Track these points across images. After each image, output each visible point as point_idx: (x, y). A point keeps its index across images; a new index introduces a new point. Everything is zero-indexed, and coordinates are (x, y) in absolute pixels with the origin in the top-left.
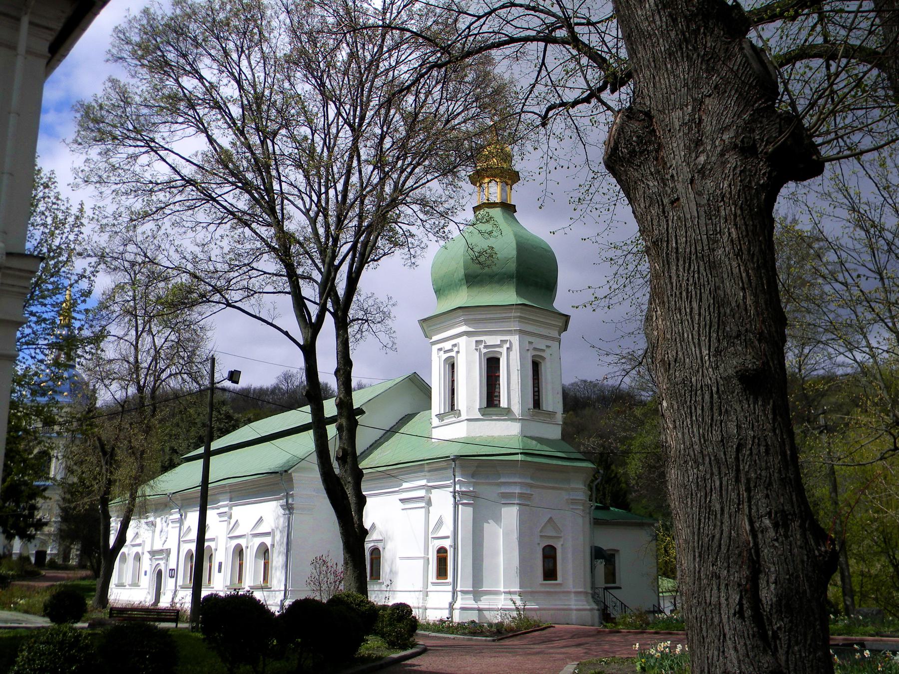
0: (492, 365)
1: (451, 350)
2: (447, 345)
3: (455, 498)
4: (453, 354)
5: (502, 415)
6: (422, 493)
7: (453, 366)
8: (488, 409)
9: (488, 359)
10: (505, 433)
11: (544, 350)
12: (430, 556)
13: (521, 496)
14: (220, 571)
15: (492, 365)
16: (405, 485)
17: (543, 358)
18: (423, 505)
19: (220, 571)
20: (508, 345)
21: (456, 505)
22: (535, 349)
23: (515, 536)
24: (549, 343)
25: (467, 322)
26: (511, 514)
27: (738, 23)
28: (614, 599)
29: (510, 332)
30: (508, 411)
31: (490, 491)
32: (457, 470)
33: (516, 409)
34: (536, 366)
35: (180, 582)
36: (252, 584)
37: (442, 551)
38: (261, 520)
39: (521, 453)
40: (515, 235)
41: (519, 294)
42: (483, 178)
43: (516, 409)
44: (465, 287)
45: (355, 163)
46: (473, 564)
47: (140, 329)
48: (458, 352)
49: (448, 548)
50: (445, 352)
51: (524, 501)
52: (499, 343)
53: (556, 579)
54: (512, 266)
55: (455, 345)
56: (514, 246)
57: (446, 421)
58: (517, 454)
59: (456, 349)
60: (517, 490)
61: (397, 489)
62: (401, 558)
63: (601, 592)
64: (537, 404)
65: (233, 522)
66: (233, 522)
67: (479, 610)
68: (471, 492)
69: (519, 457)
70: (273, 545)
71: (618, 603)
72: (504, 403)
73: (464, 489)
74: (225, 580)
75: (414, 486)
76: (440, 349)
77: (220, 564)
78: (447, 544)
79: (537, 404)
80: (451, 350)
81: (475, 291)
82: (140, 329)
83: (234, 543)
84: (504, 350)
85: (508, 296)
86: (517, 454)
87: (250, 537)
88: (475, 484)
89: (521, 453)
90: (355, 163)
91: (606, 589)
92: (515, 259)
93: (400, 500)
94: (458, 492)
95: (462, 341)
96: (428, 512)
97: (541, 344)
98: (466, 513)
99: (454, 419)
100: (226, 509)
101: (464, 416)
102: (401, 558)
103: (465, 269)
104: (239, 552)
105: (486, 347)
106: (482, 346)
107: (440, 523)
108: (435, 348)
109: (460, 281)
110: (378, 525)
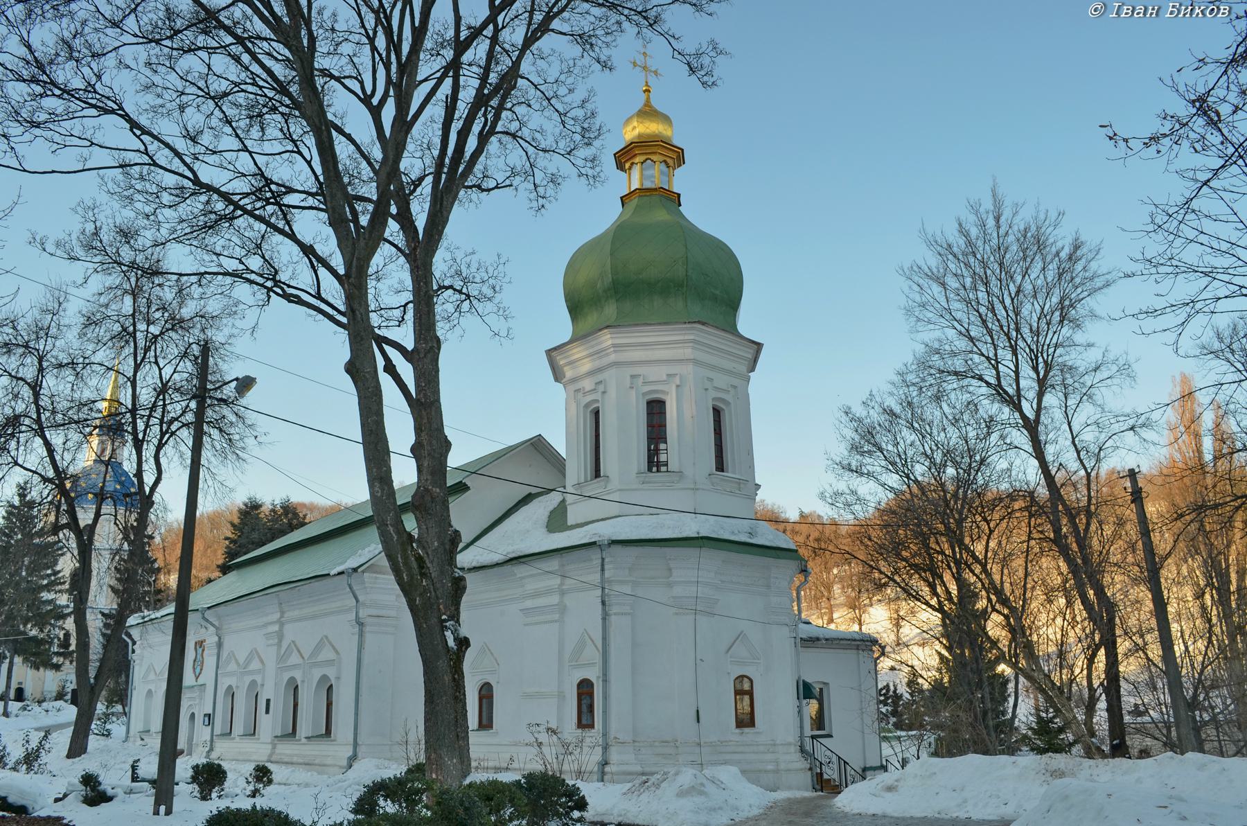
0: (656, 409)
4: (597, 396)
7: (596, 413)
14: (267, 712)
16: (531, 586)
17: (727, 403)
19: (267, 712)
22: (716, 388)
27: (6, 549)
28: (828, 753)
35: (218, 731)
45: (555, 10)
46: (426, 673)
47: (139, 359)
49: (594, 680)
59: (601, 388)
63: (808, 741)
70: (338, 678)
71: (835, 759)
77: (268, 701)
78: (593, 675)
82: (139, 359)
83: (286, 676)
90: (555, 10)
91: (813, 737)
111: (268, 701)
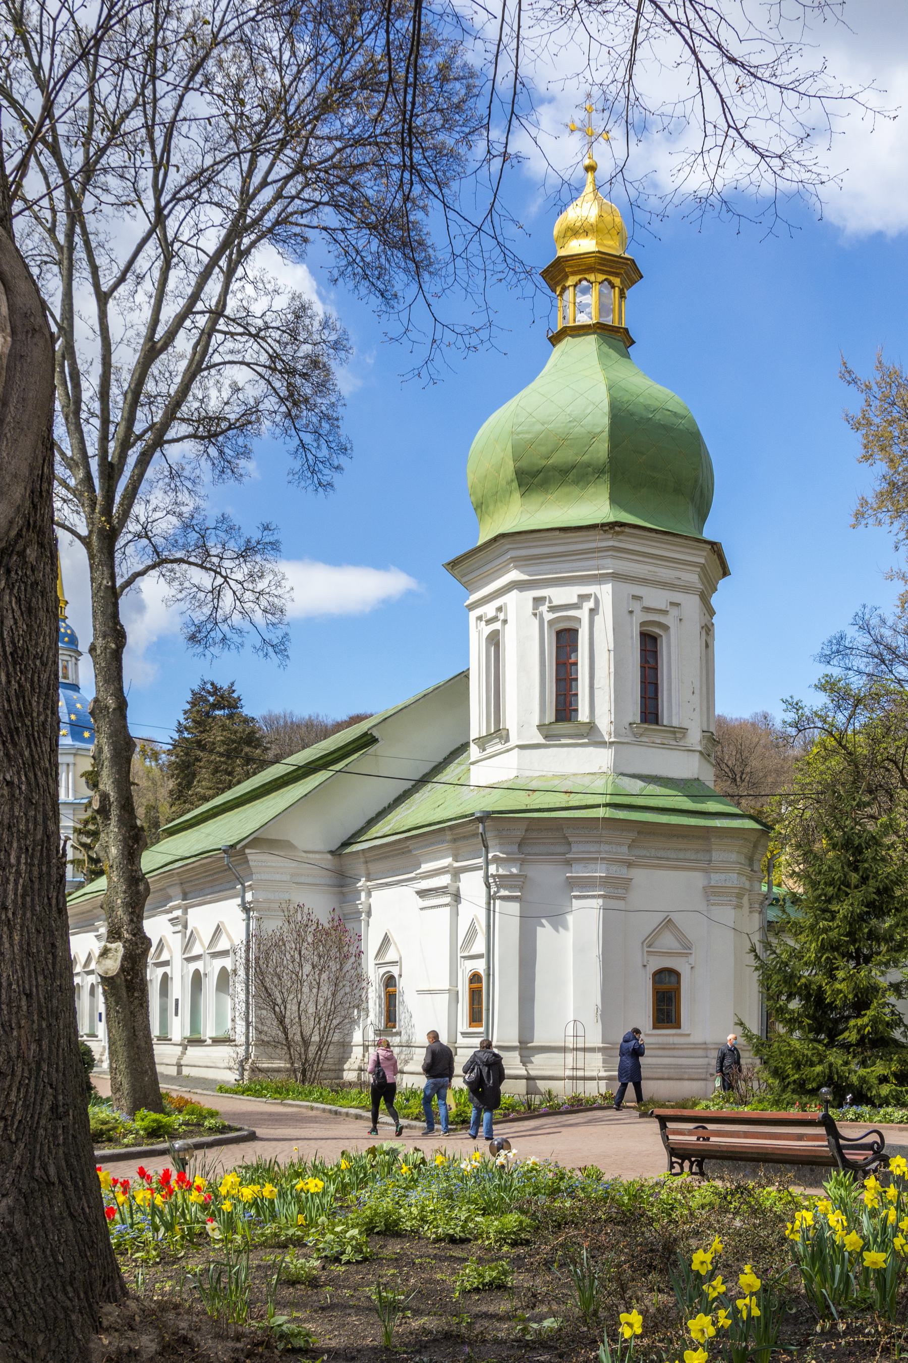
0: (565, 640)
1: (494, 619)
2: (489, 610)
3: (488, 886)
5: (581, 736)
6: (444, 880)
8: (561, 725)
9: (559, 633)
10: (583, 771)
11: (665, 612)
12: (460, 988)
13: (605, 882)
15: (565, 640)
16: (425, 867)
17: (666, 628)
18: (447, 899)
19: (176, 1014)
20: (591, 604)
21: (490, 898)
22: (647, 609)
23: (595, 951)
24: (677, 597)
25: (520, 562)
26: (586, 916)
29: (599, 579)
30: (591, 727)
31: (547, 874)
32: (489, 835)
33: (605, 723)
34: (650, 643)
36: (214, 1035)
37: (475, 978)
38: (218, 930)
39: (606, 805)
40: (610, 388)
41: (614, 500)
42: (566, 277)
43: (605, 723)
44: (517, 495)
48: (505, 622)
50: (489, 622)
51: (615, 890)
52: (575, 600)
53: (679, 1027)
54: (601, 449)
55: (500, 609)
56: (606, 409)
57: (490, 750)
58: (598, 806)
59: (502, 616)
60: (600, 872)
61: (412, 875)
62: (420, 992)
64: (650, 711)
65: (188, 933)
66: (188, 933)
67: (529, 1078)
68: (512, 876)
69: (601, 813)
72: (583, 715)
73: (501, 872)
74: (183, 1026)
75: (436, 865)
76: (480, 618)
77: (177, 1000)
78: (480, 966)
79: (650, 711)
80: (494, 619)
81: (536, 499)
83: (382, 971)
84: (583, 614)
85: (594, 507)
86: (598, 806)
87: (208, 957)
88: (523, 862)
89: (606, 805)
92: (606, 435)
93: (418, 893)
94: (493, 876)
95: (512, 599)
96: (455, 914)
97: (656, 598)
98: (509, 913)
99: (500, 746)
100: (178, 913)
101: (514, 740)
102: (420, 992)
103: (514, 461)
104: (197, 980)
105: (552, 609)
106: (544, 608)
107: (472, 933)
108: (473, 615)
109: (509, 483)
110: (394, 936)
111: (177, 1000)
